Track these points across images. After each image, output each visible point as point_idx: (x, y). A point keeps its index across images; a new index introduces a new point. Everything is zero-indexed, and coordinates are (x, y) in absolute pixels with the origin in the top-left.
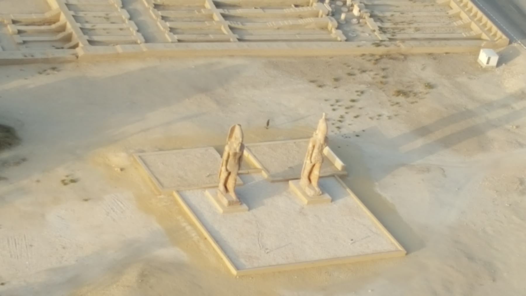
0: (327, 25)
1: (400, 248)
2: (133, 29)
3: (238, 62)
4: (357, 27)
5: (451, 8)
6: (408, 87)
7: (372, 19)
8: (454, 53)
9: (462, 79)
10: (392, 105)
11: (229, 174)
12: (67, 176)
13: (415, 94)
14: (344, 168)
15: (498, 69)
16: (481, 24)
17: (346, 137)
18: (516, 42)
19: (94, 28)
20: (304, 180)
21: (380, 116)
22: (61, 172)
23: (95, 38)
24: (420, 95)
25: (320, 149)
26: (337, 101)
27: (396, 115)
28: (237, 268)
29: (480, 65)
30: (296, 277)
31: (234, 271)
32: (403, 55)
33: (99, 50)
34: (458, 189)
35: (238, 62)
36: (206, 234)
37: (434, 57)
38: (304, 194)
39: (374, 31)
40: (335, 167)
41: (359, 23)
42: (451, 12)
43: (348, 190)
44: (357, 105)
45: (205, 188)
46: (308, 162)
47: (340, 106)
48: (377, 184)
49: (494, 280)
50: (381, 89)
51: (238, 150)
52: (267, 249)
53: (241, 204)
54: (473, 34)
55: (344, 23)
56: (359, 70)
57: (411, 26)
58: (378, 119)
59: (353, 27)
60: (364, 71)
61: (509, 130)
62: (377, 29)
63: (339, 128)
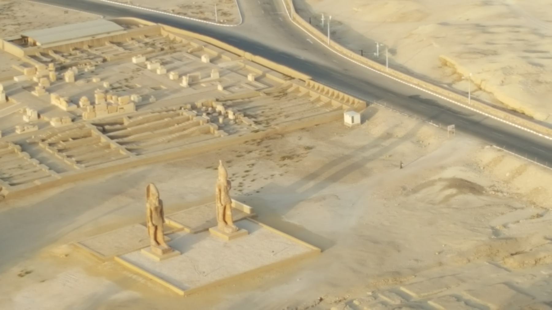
0: (209, 129)
1: (315, 249)
2: (45, 169)
3: (141, 169)
4: (236, 126)
5: (311, 97)
6: (290, 153)
7: (246, 118)
8: (323, 124)
9: (335, 138)
10: (281, 167)
11: (156, 228)
12: (22, 271)
13: (298, 156)
14: (252, 211)
15: (363, 125)
16: (339, 99)
17: (249, 195)
18: (372, 103)
19: (12, 175)
20: (221, 224)
21: (272, 175)
22: (16, 270)
23: (15, 182)
24: (302, 155)
25: (226, 191)
26: (234, 175)
27: (286, 172)
28: (183, 289)
29: (347, 126)
30: (234, 285)
31: (181, 293)
32: (279, 134)
33: (22, 187)
34: (353, 205)
35: (141, 169)
36: (150, 276)
37: (307, 130)
38: (224, 233)
39: (251, 125)
40: (245, 213)
41: (236, 123)
42: (312, 99)
43: (260, 224)
44: (251, 173)
45: (140, 249)
46: (219, 205)
47: (237, 177)
48: (283, 216)
49: (399, 251)
50: (268, 159)
51: (157, 204)
52: (204, 272)
53: (173, 251)
54: (335, 107)
55: (223, 125)
56: (245, 152)
57: (281, 115)
58: (271, 178)
59: (232, 127)
60: (250, 152)
61: (384, 160)
62: (252, 123)
63: (240, 191)
